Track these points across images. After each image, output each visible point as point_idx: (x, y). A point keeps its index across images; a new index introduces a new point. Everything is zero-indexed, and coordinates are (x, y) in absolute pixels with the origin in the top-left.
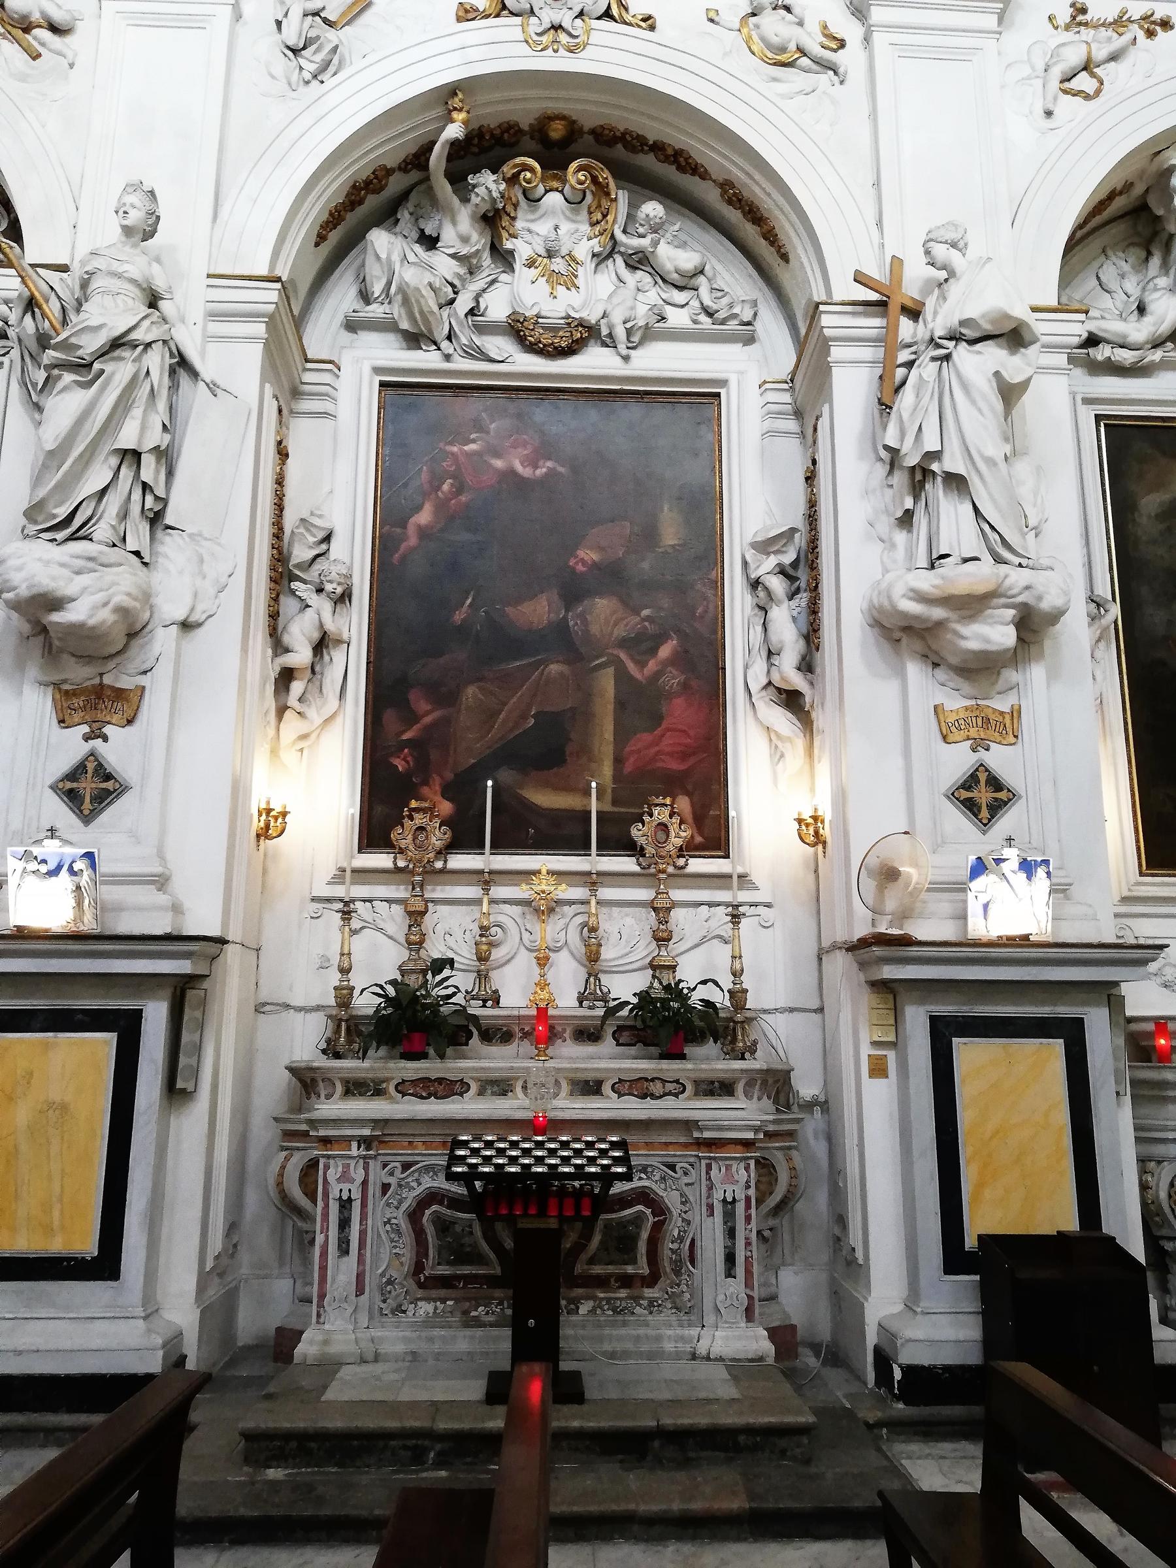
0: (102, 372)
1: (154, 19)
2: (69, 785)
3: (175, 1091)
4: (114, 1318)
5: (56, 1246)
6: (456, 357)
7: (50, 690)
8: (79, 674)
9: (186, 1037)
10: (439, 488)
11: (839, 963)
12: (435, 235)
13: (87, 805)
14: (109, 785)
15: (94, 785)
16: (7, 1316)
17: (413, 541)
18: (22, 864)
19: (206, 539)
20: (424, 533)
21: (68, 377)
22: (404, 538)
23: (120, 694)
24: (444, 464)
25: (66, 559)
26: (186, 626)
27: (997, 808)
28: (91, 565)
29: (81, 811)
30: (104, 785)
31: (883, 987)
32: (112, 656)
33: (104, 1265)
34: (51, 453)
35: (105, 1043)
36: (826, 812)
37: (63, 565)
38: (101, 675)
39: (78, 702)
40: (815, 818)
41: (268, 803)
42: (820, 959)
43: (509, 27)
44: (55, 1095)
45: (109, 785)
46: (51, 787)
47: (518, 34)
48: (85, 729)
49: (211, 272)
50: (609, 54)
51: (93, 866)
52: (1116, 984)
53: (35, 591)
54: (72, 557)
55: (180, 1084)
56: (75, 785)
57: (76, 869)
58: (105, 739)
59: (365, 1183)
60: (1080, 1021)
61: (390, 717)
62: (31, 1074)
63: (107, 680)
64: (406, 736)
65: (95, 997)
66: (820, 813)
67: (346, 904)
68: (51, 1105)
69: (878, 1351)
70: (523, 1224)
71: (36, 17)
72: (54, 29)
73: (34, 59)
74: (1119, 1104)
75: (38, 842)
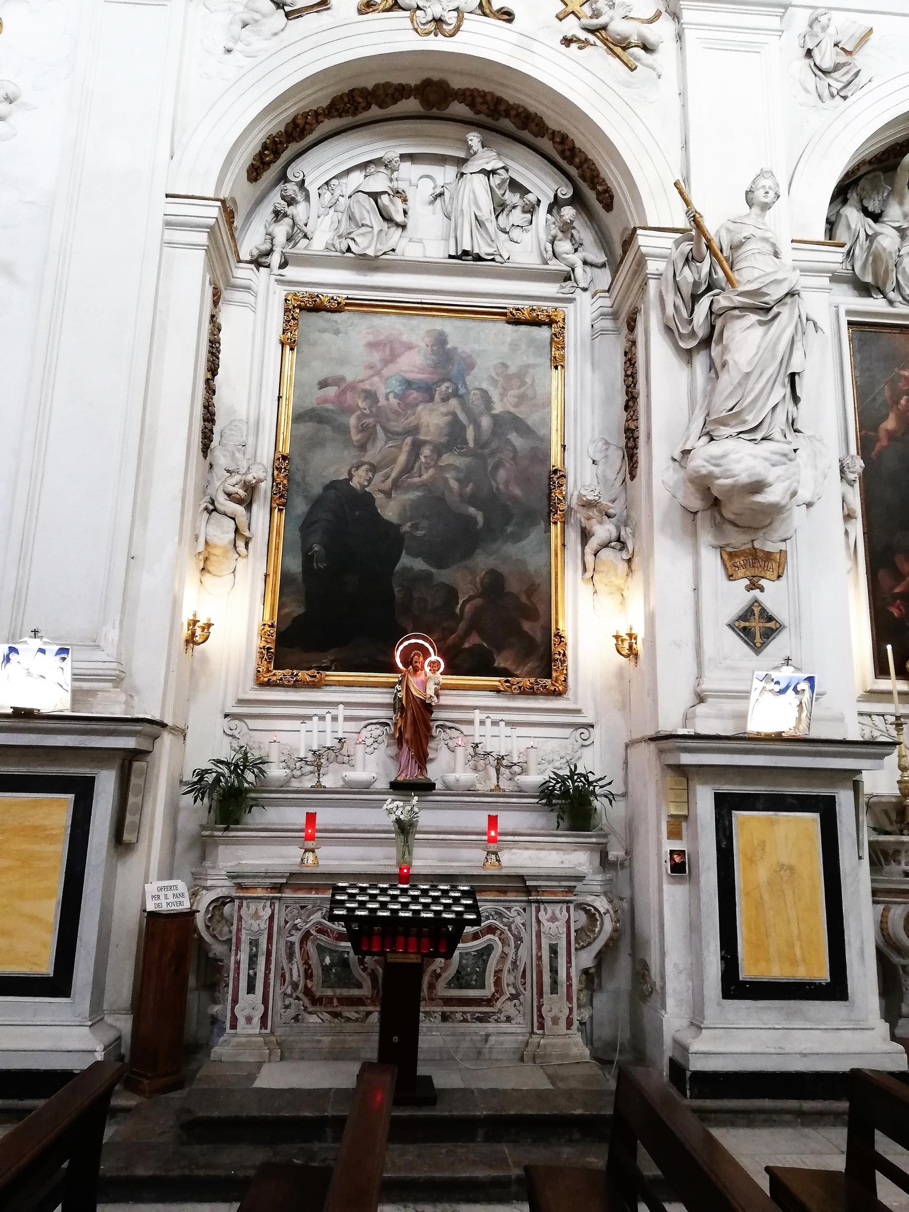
0: (778, 314)
1: (722, 45)
2: (743, 624)
3: (121, 843)
4: (854, 1029)
5: (801, 973)
6: (897, 304)
7: (718, 551)
8: (739, 540)
9: (132, 799)
10: (897, 402)
11: (646, 754)
12: (878, 211)
13: (758, 639)
14: (771, 625)
15: (761, 625)
16: (777, 1026)
17: (884, 442)
18: (763, 684)
19: (817, 440)
20: (891, 435)
21: (753, 318)
22: (878, 440)
23: (768, 556)
24: (900, 384)
25: (768, 455)
26: (809, 505)
27: (769, 634)
28: (784, 459)
29: (755, 644)
30: (768, 625)
31: (681, 770)
32: (766, 526)
33: (735, 987)
34: (748, 375)
35: (812, 819)
36: (640, 632)
37: (766, 459)
38: (753, 541)
39: (740, 561)
40: (630, 636)
41: (195, 615)
42: (626, 749)
43: (400, 18)
44: (784, 860)
45: (771, 625)
46: (729, 625)
47: (407, 23)
48: (746, 582)
49: (795, 238)
50: (480, 40)
51: (812, 688)
52: (859, 772)
53: (754, 479)
54: (772, 453)
55: (127, 837)
56: (747, 624)
57: (799, 689)
58: (762, 589)
59: (271, 918)
60: (93, 779)
61: (882, 574)
62: (764, 842)
63: (757, 545)
64: (897, 590)
65: (800, 786)
66: (633, 632)
67: (898, 718)
68: (782, 866)
69: (672, 1061)
70: (392, 958)
71: (634, 39)
72: (646, 48)
73: (632, 70)
74: (860, 864)
75: (776, 668)
